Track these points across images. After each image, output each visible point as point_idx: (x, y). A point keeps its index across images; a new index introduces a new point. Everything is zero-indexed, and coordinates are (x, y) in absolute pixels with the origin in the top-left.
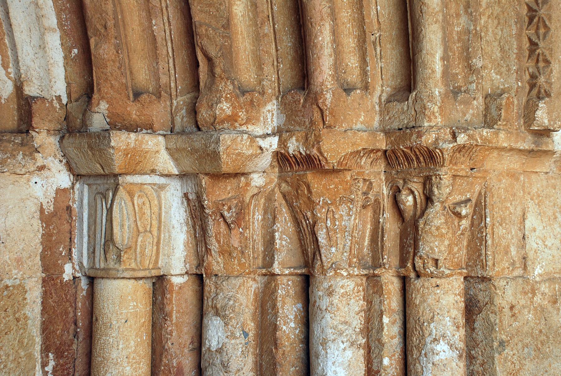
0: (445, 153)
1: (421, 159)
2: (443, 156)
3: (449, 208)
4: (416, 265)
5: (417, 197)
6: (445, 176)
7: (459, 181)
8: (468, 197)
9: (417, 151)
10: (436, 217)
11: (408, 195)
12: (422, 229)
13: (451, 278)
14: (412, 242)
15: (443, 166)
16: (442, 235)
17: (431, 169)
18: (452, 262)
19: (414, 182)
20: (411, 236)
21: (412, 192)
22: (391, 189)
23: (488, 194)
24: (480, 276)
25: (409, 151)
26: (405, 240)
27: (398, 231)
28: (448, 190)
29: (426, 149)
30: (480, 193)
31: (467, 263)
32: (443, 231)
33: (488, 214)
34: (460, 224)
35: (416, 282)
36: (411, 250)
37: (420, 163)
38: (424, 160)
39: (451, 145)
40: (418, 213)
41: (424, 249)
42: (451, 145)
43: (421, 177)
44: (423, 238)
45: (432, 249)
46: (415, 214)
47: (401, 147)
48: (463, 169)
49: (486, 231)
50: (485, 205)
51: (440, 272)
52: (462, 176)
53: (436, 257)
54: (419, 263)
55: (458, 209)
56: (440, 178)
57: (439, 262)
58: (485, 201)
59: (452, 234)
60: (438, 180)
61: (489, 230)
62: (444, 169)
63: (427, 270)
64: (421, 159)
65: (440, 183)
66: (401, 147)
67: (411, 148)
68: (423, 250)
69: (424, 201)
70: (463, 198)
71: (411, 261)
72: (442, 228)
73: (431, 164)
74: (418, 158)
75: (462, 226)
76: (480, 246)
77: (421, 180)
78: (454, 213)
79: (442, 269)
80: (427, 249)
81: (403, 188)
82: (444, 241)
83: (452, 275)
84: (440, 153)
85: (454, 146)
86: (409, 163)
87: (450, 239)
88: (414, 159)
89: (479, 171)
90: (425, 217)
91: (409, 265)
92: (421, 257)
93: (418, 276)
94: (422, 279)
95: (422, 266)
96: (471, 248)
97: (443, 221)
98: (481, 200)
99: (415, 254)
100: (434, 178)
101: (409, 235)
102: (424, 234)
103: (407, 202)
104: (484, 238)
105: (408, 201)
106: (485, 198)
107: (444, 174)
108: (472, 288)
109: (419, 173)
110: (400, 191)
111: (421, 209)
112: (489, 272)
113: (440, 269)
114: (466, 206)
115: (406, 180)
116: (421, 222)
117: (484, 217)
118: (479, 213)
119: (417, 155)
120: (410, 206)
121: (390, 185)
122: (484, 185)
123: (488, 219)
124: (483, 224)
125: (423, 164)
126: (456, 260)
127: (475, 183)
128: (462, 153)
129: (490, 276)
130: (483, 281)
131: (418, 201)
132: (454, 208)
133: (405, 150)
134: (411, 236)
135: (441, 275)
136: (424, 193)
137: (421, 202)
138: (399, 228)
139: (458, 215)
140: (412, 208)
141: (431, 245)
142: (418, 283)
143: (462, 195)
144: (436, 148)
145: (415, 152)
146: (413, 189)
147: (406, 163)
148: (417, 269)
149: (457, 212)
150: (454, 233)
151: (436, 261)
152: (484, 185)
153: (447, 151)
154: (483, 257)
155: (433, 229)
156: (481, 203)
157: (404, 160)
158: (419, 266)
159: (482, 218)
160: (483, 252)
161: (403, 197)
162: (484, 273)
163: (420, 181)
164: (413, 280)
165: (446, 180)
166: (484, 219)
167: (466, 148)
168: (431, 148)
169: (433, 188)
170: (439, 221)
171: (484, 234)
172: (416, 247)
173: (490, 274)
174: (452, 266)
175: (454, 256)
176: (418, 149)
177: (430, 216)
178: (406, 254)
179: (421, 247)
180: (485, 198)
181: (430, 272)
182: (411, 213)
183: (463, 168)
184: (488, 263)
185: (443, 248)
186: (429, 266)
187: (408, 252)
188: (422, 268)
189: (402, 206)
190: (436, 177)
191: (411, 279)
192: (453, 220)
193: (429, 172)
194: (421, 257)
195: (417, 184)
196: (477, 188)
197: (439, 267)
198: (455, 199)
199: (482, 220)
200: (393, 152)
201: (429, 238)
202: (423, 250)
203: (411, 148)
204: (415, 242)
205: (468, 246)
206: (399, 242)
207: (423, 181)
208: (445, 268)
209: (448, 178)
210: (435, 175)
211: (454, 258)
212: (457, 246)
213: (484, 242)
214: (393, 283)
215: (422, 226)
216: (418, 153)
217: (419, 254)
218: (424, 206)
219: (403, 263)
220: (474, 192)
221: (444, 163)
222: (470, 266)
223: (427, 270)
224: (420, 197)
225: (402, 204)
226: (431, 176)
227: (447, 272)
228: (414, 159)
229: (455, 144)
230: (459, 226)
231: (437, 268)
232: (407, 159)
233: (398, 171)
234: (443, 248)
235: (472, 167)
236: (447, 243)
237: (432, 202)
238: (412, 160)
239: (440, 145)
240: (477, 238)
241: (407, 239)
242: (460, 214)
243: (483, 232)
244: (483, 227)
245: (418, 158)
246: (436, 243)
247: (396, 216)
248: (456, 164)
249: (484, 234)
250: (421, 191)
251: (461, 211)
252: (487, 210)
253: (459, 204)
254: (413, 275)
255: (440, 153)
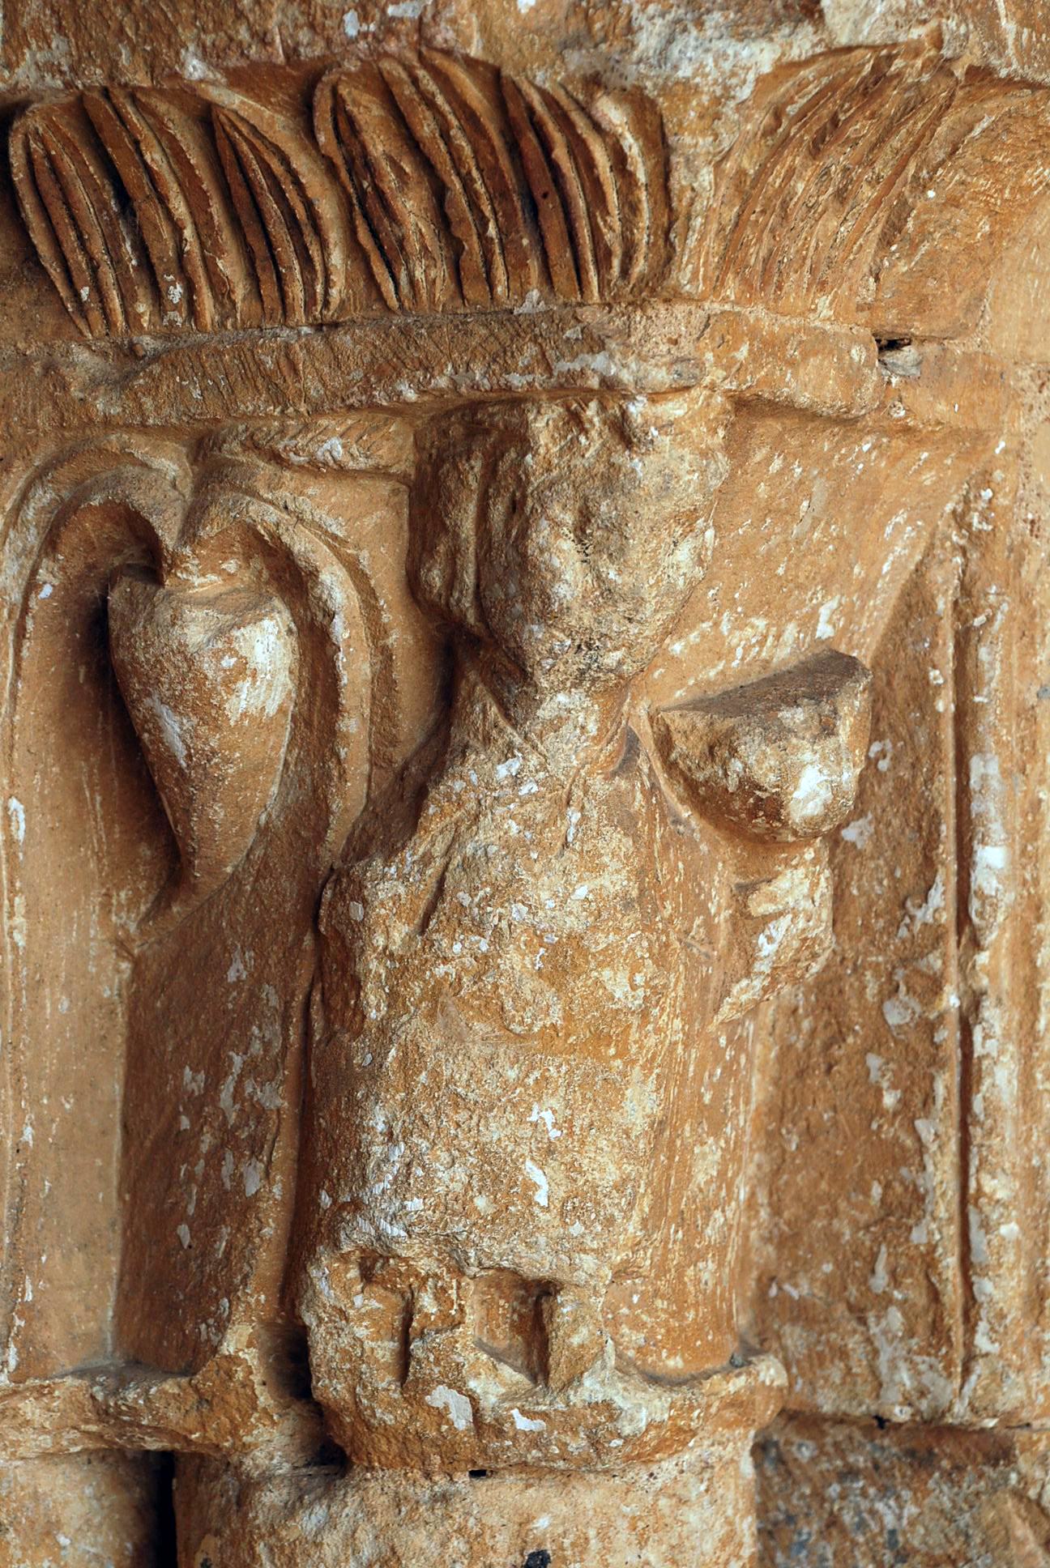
0: (691, 142)
1: (412, 210)
2: (664, 172)
3: (665, 743)
4: (324, 1347)
5: (340, 631)
6: (674, 409)
7: (772, 462)
8: (824, 630)
9: (368, 112)
10: (551, 836)
11: (247, 611)
12: (402, 968)
13: (667, 1468)
14: (277, 1099)
15: (656, 287)
16: (602, 1033)
17: (518, 328)
18: (679, 1297)
19: (315, 468)
20: (265, 1036)
21: (290, 579)
22: (50, 543)
23: (999, 608)
24: (900, 1414)
25: (277, 125)
26: (192, 1080)
27: (111, 978)
28: (684, 554)
29: (474, 94)
30: (914, 601)
31: (767, 1280)
32: (619, 986)
33: (988, 807)
34: (759, 906)
35: (309, 1521)
36: (267, 1187)
37: (393, 254)
38: (443, 221)
39: (762, 56)
40: (351, 797)
41: (416, 1181)
42: (762, 56)
43: (400, 410)
44: (407, 1066)
45: (496, 1173)
46: (310, 812)
47: (195, 68)
48: (819, 343)
49: (966, 968)
50: (964, 716)
51: (569, 1422)
52: (808, 416)
53: (539, 1263)
54: (350, 1325)
55: (756, 759)
56: (623, 433)
57: (566, 1306)
58: (964, 679)
59: (688, 1016)
60: (593, 442)
61: (993, 961)
62: (665, 325)
63: (440, 1396)
64: (412, 210)
65: (611, 480)
66: (195, 68)
67: (304, 89)
68: (402, 1185)
69: (410, 676)
70: (786, 648)
71: (258, 1298)
72: (608, 958)
73: (516, 268)
74: (367, 207)
75: (780, 929)
76: (907, 1113)
77: (394, 447)
78: (710, 801)
79: (591, 1388)
80: (451, 1178)
81: (189, 533)
82: (615, 1090)
83: (675, 1437)
84: (632, 145)
85: (786, 68)
86: (261, 262)
87: (670, 1074)
88: (328, 209)
89: (938, 373)
90: (431, 839)
91: (242, 1343)
92: (374, 1266)
93: (331, 1453)
94: (377, 1489)
95: (385, 1350)
96: (810, 1136)
97: (615, 880)
98: (924, 662)
99: (306, 1234)
100: (544, 425)
101: (243, 1021)
102: (413, 1025)
103: (230, 681)
104: (949, 1035)
105: (243, 669)
106: (964, 642)
107: (661, 376)
108: (809, 1529)
109: (383, 371)
110: (151, 564)
111: (376, 759)
112: (998, 1377)
113: (573, 1380)
114: (827, 730)
115: (232, 449)
116: (390, 894)
117: (947, 830)
118: (903, 789)
119: (360, 164)
120: (259, 723)
121: (43, 497)
122: (960, 519)
123: (992, 857)
124: (941, 898)
125: (429, 272)
126: (707, 1270)
127: (887, 495)
128: (837, 159)
129: (1009, 1420)
130: (921, 1460)
131: (355, 669)
132: (719, 747)
133: (233, 100)
134: (265, 1036)
135: (578, 1444)
136: (413, 584)
137: (384, 681)
138: (122, 946)
139: (751, 821)
140: (279, 746)
141: (495, 1131)
142: (332, 1541)
143: (778, 613)
144: (594, 82)
145: (346, 127)
146: (302, 543)
147: (229, 265)
148: (331, 1388)
149: (749, 785)
150: (702, 1002)
151: (533, 1305)
152: (960, 519)
153: (712, 116)
154: (936, 1229)
155: (516, 961)
156: (922, 694)
157: (204, 228)
158: (355, 1359)
159: (931, 842)
160: (941, 1173)
161: (195, 631)
162: (945, 1389)
163: (384, 454)
164: (272, 1497)
165: (679, 447)
166: (947, 850)
167: (891, 101)
168: (541, 79)
169: (541, 533)
170: (565, 894)
171: (951, 1000)
172: (323, 1156)
173: (1011, 1396)
174: (678, 1340)
175: (694, 1232)
176: (386, 93)
177: (486, 836)
178: (206, 1224)
179: (386, 1161)
180: (964, 642)
181: (461, 1419)
182: (268, 796)
183: (818, 337)
184: (986, 1287)
185: (605, 1166)
186: (467, 1356)
187: (234, 1207)
188: (385, 1381)
189: (175, 729)
190: (575, 419)
191: (247, 1489)
192: (694, 874)
193: (501, 358)
194: (374, 1266)
195: (342, 493)
196: (898, 547)
197: (559, 1359)
198: (717, 649)
199: (929, 864)
200: (92, 122)
201: (468, 1061)
202: (402, 1185)
203: (304, 89)
204: (307, 1103)
205: (779, 1112)
206: (114, 1088)
207: (405, 463)
208: (624, 1368)
209: (699, 430)
210: (571, 394)
211: (694, 1256)
212: (716, 1130)
213: (945, 1084)
214: (51, 1528)
215: (400, 932)
216: (379, 144)
217: (358, 1234)
218: (410, 724)
219: (163, 1313)
220: (867, 588)
221: (667, 258)
222: (801, 1313)
223: (440, 1396)
224: (377, 631)
225: (176, 703)
226: (516, 402)
227: (644, 1409)
228: (328, 209)
229: (804, 42)
230: (747, 925)
231: (538, 1365)
232: (247, 218)
233: (131, 352)
234: (605, 1166)
235: (890, 320)
236: (640, 1104)
237: (512, 678)
238: (305, 227)
239: (648, 41)
240: (880, 1037)
241: (216, 1071)
242: (773, 808)
243: (936, 985)
244: (936, 936)
245: (367, 207)
246: (545, 1114)
247: (96, 828)
248: (767, 279)
249: (951, 1000)
250: (384, 564)
251: (789, 775)
252: (985, 768)
253: (759, 698)
254: (270, 1444)
255: (632, 145)
